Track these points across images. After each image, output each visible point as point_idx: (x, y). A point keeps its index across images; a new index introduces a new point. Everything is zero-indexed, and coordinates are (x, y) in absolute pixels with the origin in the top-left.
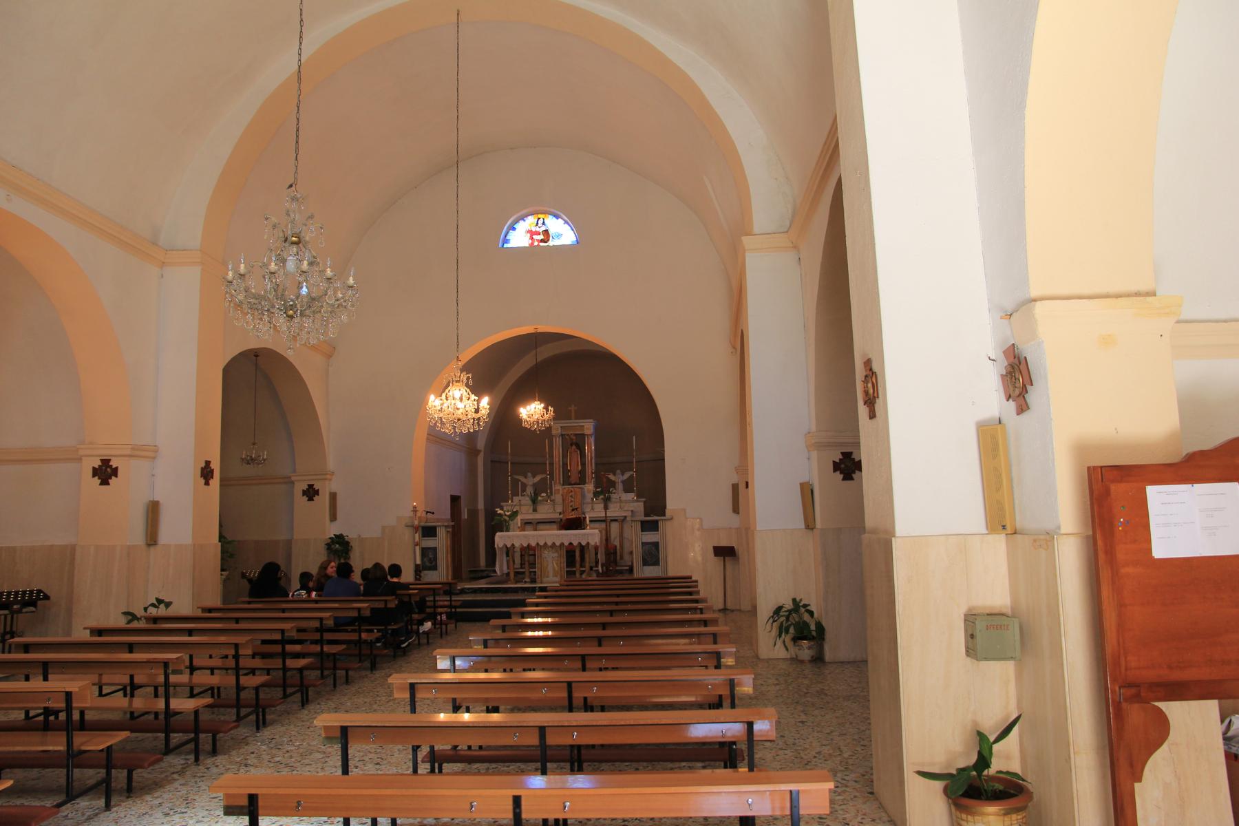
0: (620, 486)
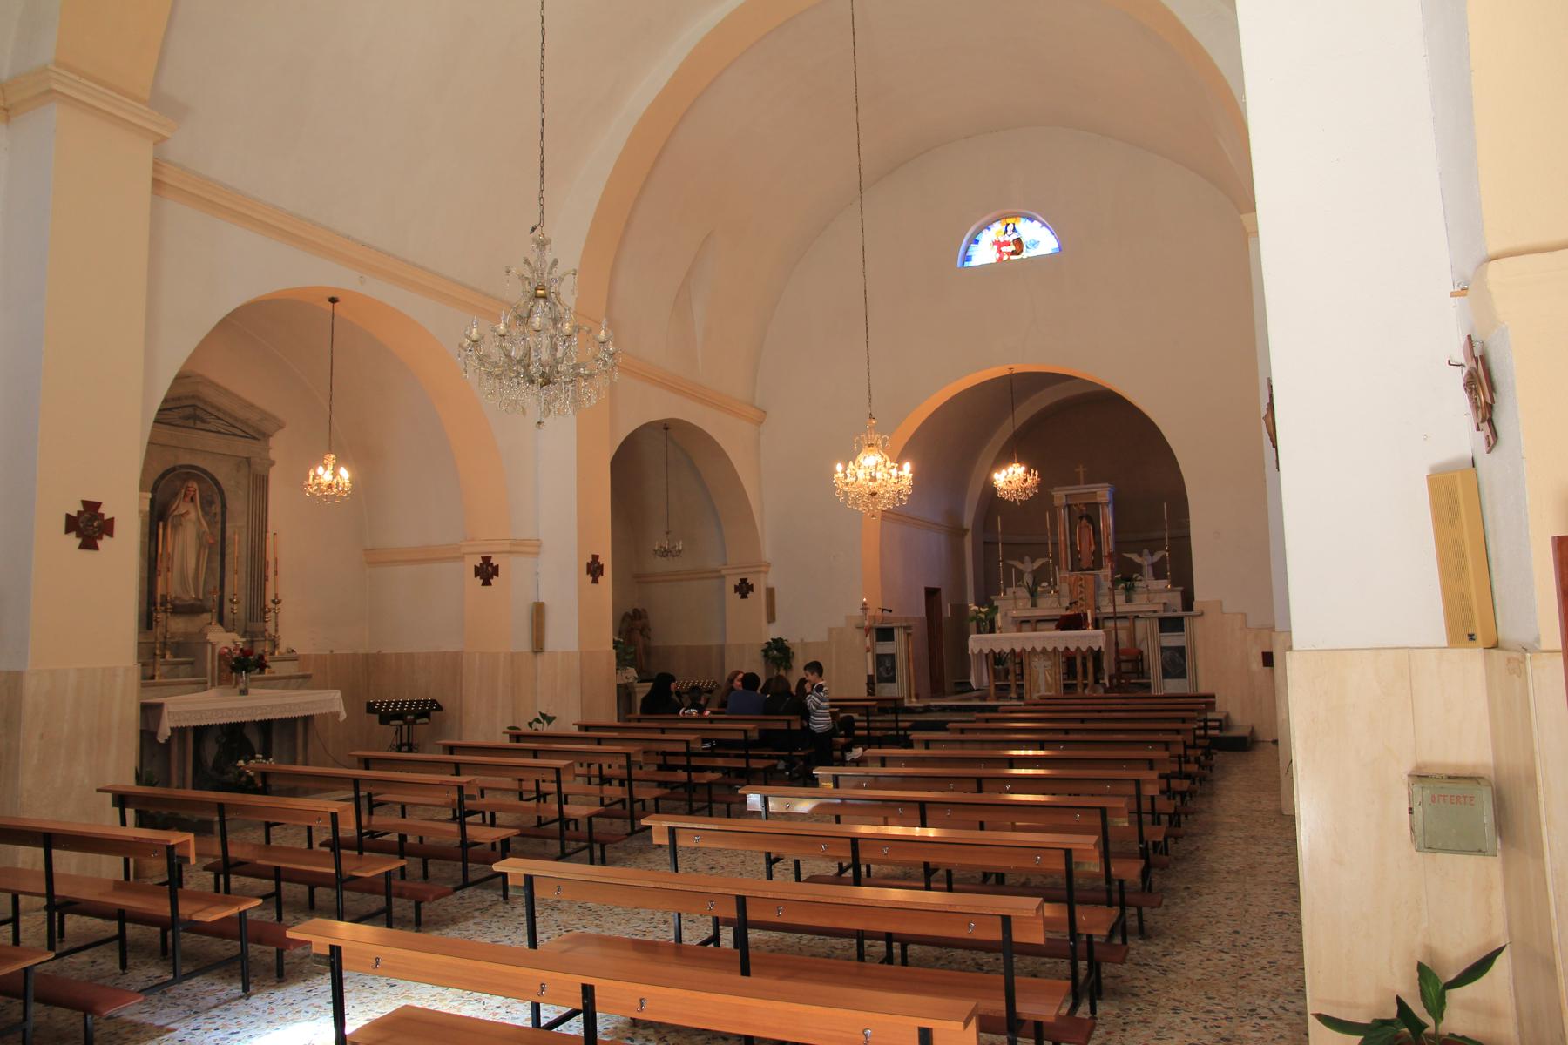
0: (1148, 571)
